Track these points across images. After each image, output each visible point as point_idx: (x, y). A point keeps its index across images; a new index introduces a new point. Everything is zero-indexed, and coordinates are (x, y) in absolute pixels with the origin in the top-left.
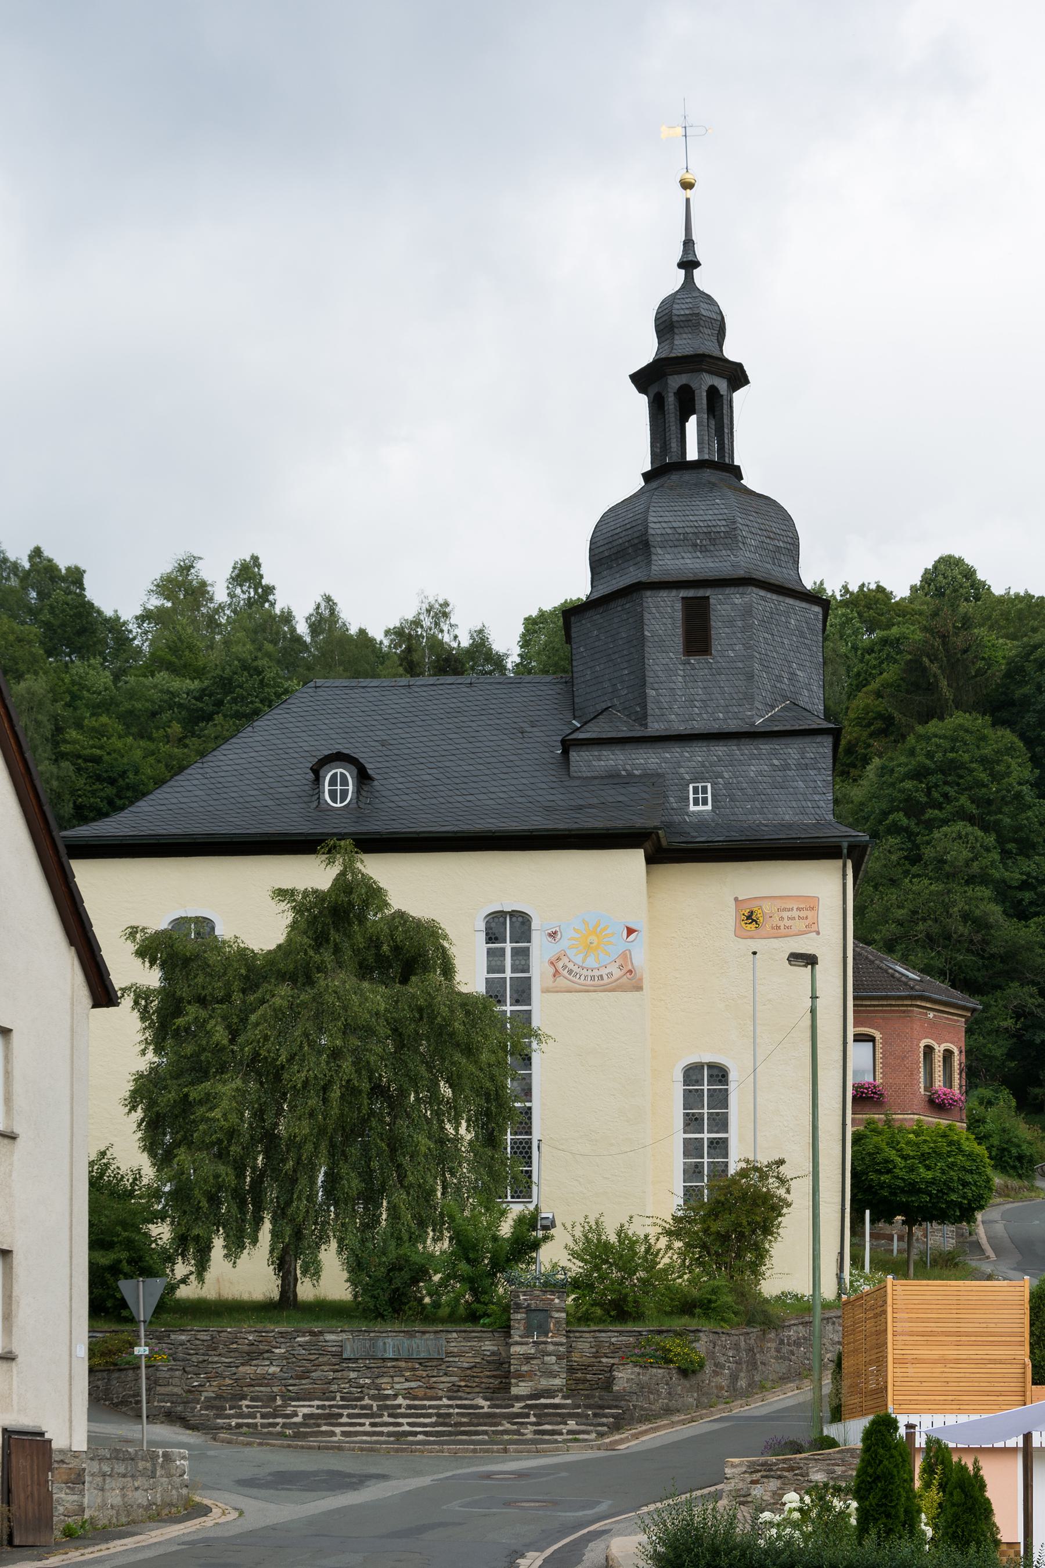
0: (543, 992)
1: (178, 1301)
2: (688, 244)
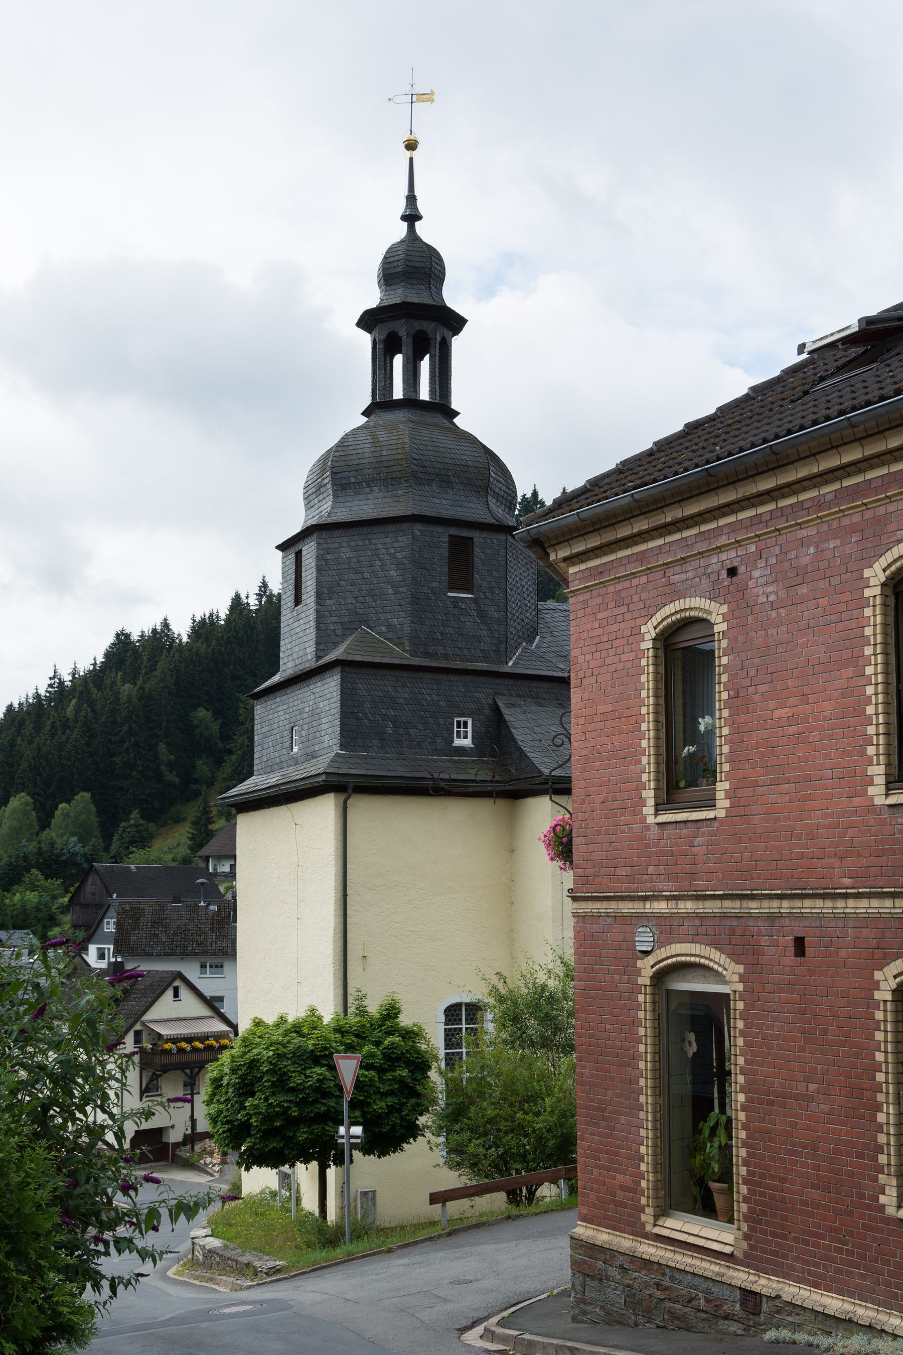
0: (564, 682)
1: (456, 747)
2: (411, 199)
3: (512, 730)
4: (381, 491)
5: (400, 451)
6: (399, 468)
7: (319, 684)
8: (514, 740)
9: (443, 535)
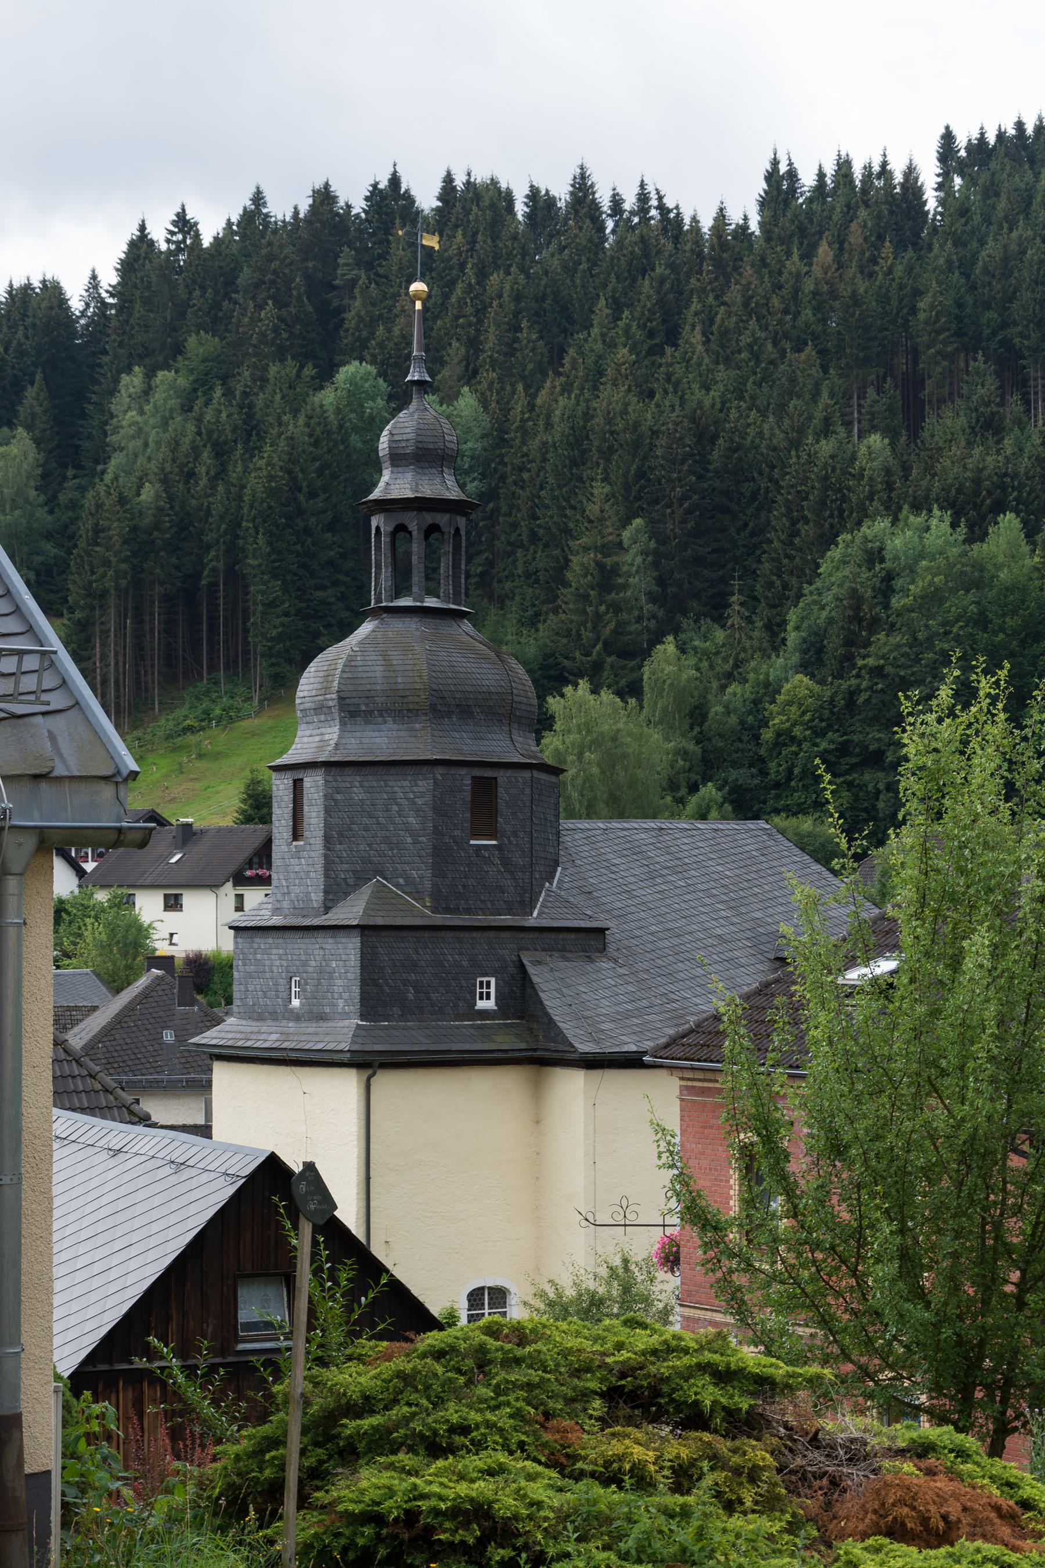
3: (541, 994)
4: (395, 722)
5: (417, 679)
6: (417, 700)
7: (330, 940)
8: (541, 1003)
9: (465, 778)
